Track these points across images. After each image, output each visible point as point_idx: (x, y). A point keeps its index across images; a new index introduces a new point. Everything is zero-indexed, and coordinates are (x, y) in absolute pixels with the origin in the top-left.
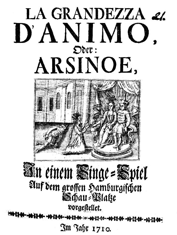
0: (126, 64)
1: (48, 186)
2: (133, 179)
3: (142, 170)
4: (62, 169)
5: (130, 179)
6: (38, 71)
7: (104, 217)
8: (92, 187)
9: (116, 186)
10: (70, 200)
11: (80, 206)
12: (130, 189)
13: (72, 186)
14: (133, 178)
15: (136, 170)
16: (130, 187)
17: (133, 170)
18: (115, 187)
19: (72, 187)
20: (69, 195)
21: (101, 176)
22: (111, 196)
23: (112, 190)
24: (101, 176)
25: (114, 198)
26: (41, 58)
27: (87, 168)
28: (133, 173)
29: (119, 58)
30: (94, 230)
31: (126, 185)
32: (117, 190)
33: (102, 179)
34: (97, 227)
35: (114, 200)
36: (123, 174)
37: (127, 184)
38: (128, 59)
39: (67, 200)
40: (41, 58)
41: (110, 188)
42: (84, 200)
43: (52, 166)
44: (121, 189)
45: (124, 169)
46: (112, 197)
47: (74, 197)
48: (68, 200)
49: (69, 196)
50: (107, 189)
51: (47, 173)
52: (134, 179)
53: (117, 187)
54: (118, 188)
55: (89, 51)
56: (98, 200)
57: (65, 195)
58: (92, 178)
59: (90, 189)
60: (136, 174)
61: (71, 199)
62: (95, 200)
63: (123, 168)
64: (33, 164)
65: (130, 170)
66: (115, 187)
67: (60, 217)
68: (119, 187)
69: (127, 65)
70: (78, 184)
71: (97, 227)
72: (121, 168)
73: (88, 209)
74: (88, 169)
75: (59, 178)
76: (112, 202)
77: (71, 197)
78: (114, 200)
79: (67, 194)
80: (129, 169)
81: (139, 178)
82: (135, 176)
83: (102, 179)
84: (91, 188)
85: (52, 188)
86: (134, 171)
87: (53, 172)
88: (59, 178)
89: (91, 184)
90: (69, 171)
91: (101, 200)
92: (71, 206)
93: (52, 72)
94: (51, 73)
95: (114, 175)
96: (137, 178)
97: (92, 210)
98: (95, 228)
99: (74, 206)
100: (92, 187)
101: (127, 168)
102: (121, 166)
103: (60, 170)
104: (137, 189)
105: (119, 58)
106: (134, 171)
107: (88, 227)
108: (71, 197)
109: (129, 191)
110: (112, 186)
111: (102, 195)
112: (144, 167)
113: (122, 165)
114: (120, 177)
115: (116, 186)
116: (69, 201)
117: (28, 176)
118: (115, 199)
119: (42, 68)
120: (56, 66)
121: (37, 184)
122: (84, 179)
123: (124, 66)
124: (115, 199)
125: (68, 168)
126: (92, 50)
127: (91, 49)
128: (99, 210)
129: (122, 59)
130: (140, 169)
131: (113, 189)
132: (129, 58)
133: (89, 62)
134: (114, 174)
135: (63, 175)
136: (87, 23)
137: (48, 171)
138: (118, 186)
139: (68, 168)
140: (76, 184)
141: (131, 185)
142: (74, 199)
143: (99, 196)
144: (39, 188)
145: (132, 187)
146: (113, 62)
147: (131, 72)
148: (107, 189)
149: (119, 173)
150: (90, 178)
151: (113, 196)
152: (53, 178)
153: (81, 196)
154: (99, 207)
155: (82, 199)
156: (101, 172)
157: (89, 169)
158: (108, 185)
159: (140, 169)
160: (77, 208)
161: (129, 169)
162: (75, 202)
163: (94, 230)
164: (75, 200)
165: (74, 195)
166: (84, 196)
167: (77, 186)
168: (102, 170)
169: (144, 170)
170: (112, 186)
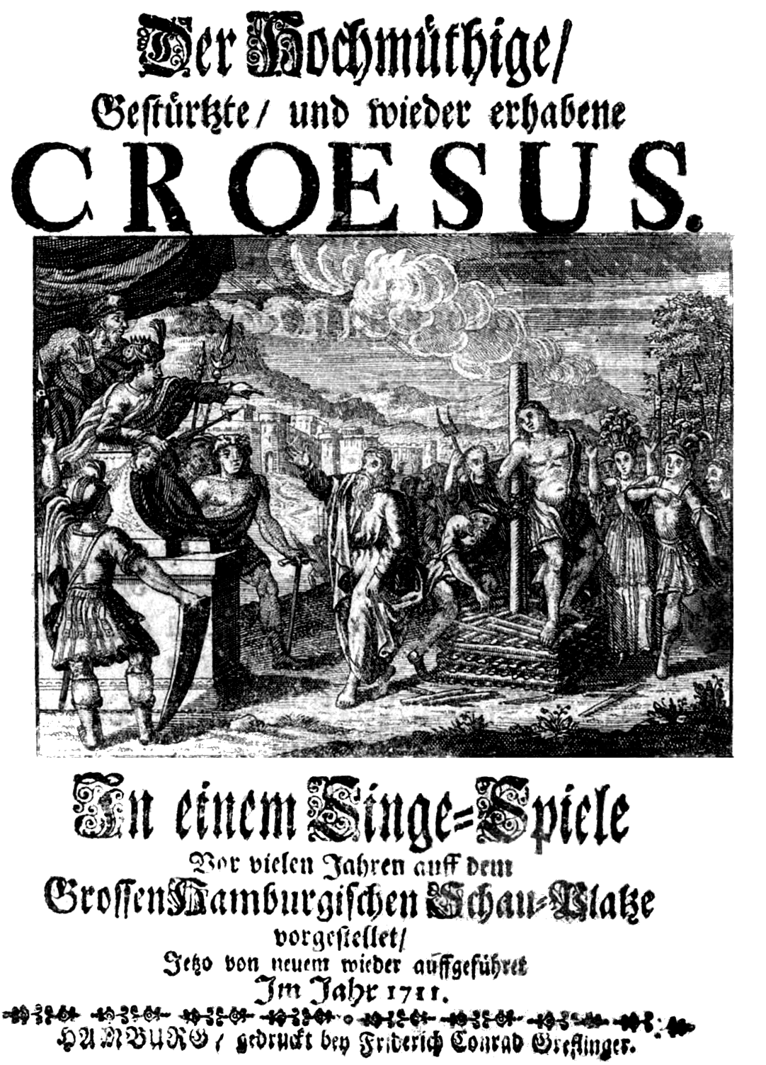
3: (586, 803)
4: (250, 798)
7: (425, 1013)
10: (458, 913)
13: (105, 890)
14: (548, 837)
19: (104, 894)
20: (453, 891)
21: (516, 63)
22: (635, 894)
24: (516, 63)
25: (644, 904)
27: (354, 793)
28: (547, 811)
30: (391, 997)
31: (349, 888)
32: (307, 912)
33: (519, 77)
34: (403, 988)
35: (647, 913)
39: (447, 917)
41: (276, 901)
43: (206, 784)
46: (639, 901)
47: (476, 901)
48: (449, 914)
50: (261, 906)
51: (180, 817)
54: (313, 904)
55: (218, 59)
56: (574, 915)
57: (437, 893)
58: (377, 836)
61: (465, 911)
62: (560, 911)
63: (501, 794)
64: (114, 780)
65: (532, 799)
70: (133, 882)
71: (403, 988)
74: (357, 798)
76: (636, 921)
77: (465, 900)
78: (647, 913)
80: (527, 794)
82: (552, 826)
83: (421, 842)
85: (589, 116)
86: (551, 803)
87: (210, 807)
88: (238, 835)
91: (588, 913)
96: (566, 835)
98: (397, 992)
102: (492, 784)
103: (239, 800)
106: (551, 803)
107: (468, 106)
108: (465, 900)
111: (594, 891)
113: (326, 779)
115: (304, 893)
116: (455, 916)
117: (93, 835)
118: (626, 830)
124: (626, 830)
126: (466, 115)
127: (227, 42)
131: (289, 907)
134: (461, 820)
135: (254, 819)
138: (313, 894)
140: (122, 882)
141: (371, 888)
143: (578, 896)
148: (261, 906)
150: (369, 834)
151: (641, 894)
155: (515, 907)
156: (517, 42)
157: (364, 796)
159: (409, 104)
160: (309, 939)
161: (527, 794)
162: (483, 922)
163: (391, 997)
164: (481, 912)
167: (128, 891)
168: (422, 801)
169: (593, 801)
170: (285, 894)
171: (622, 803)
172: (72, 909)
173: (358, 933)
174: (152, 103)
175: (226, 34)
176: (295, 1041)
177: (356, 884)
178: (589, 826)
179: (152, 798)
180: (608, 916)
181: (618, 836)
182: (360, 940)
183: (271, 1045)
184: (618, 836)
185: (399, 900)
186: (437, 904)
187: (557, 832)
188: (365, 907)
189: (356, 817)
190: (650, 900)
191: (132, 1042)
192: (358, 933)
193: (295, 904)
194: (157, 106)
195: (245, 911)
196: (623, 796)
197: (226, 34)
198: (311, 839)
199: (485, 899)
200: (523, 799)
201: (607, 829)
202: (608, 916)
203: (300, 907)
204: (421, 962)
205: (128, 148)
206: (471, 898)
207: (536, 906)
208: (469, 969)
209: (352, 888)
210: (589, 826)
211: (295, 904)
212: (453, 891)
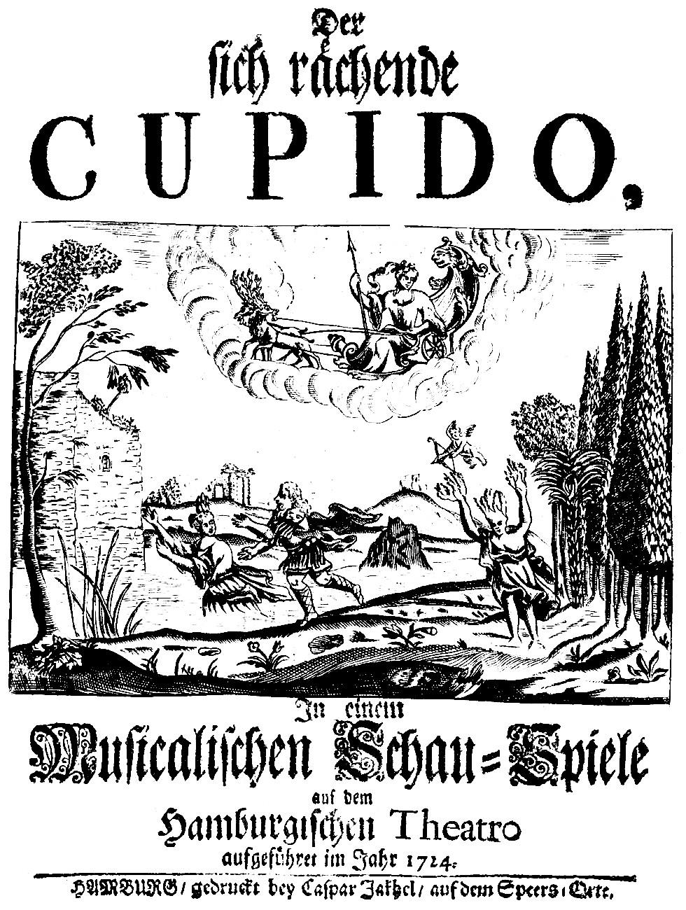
2: (572, 782)
3: (610, 746)
5: (562, 783)
8: (176, 824)
9: (272, 818)
15: (585, 745)
16: (327, 825)
17: (572, 745)
18: (268, 823)
23: (254, 836)
28: (575, 754)
30: (410, 865)
34: (419, 858)
36: (532, 762)
44: (290, 831)
45: (361, 739)
50: (233, 831)
52: (577, 781)
53: (276, 823)
59: (165, 831)
60: (424, 762)
65: (562, 744)
66: (268, 823)
67: (411, 876)
71: (419, 858)
73: (627, 778)
75: (149, 775)
81: (599, 778)
84: (170, 829)
89: (171, 810)
90: (295, 746)
95: (498, 765)
96: (592, 780)
97: (230, 892)
100: (176, 824)
101: (373, 733)
102: (525, 731)
110: (253, 819)
112: (619, 735)
114: (519, 775)
115: (272, 818)
122: (539, 782)
124: (646, 771)
125: (568, 742)
127: (300, 63)
128: (285, 739)
130: (601, 742)
131: (258, 831)
134: (494, 761)
136: (419, 115)
137: (608, 754)
139: (568, 742)
144: (241, 863)
149: (517, 757)
152: (450, 779)
158: (238, 814)
159: (601, 742)
161: (557, 740)
163: (410, 865)
169: (617, 744)
170: (253, 819)
171: (643, 749)
175: (299, 57)
177: (318, 811)
178: (613, 765)
179: (310, 742)
181: (638, 778)
185: (311, 859)
187: (584, 776)
189: (555, 761)
191: (123, 891)
193: (304, 829)
195: (219, 836)
196: (160, 737)
197: (299, 57)
198: (514, 783)
201: (628, 771)
203: (268, 831)
204: (228, 854)
205: (252, 117)
207: (477, 764)
208: (267, 861)
210: (613, 765)
211: (304, 829)
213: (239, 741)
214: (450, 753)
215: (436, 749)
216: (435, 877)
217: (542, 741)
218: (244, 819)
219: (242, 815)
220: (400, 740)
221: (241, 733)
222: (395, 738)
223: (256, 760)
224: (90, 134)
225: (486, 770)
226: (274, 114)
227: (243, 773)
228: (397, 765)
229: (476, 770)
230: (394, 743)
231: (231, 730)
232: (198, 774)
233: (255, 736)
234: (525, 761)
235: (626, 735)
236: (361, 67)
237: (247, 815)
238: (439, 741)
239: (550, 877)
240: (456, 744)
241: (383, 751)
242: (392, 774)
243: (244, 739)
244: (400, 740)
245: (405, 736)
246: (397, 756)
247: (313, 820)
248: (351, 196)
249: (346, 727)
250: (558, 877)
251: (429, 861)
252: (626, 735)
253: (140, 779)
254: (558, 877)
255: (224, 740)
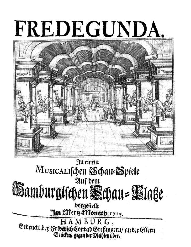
0: (48, 28)
1: (91, 180)
6: (151, 36)
11: (59, 189)
12: (71, 195)
18: (51, 191)
20: (122, 169)
24: (58, 195)
26: (153, 22)
29: (41, 22)
33: (59, 198)
34: (113, 213)
37: (73, 167)
38: (50, 23)
40: (153, 22)
42: (110, 174)
47: (100, 171)
48: (121, 174)
49: (95, 170)
63: (96, 188)
66: (51, 191)
68: (83, 205)
69: (49, 29)
72: (94, 188)
79: (94, 168)
83: (59, 198)
90: (35, 190)
92: (77, 204)
93: (73, 35)
94: (42, 36)
99: (79, 204)
104: (82, 172)
105: (41, 22)
109: (74, 174)
111: (145, 189)
118: (139, 173)
119: (155, 32)
120: (32, 29)
121: (82, 180)
123: (77, 30)
124: (139, 173)
129: (75, 23)
132: (82, 22)
133: (121, 26)
138: (82, 205)
142: (100, 173)
144: (83, 183)
145: (77, 170)
146: (66, 26)
147: (84, 36)
153: (107, 170)
154: (99, 205)
155: (108, 172)
160: (82, 206)
162: (101, 176)
163: (111, 215)
165: (100, 169)
166: (110, 170)
172: (58, 236)
173: (93, 205)
174: (90, 205)
176: (64, 235)
180: (127, 169)
181: (138, 174)
182: (93, 207)
183: (59, 236)
184: (138, 174)
186: (92, 172)
188: (75, 173)
190: (138, 171)
192: (93, 205)
194: (91, 205)
199: (102, 170)
200: (101, 190)
202: (127, 169)
206: (99, 171)
207: (113, 172)
209: (67, 188)
210: (133, 172)
212: (95, 169)
213: (70, 190)
214: (118, 193)
215: (114, 192)
216: (128, 218)
217: (98, 189)
218: (43, 189)
219: (42, 187)
220: (106, 190)
221: (71, 188)
222: (105, 190)
223: (75, 195)
224: (52, 24)
225: (126, 196)
226: (138, 22)
227: (71, 197)
228: (105, 196)
229: (124, 196)
230: (105, 191)
231: (68, 187)
232: (31, 196)
233: (74, 189)
234: (94, 194)
235: (146, 188)
236: (109, 192)
237: (44, 187)
238: (115, 190)
239: (121, 218)
240: (119, 191)
241: (102, 192)
242: (104, 198)
243: (72, 190)
244: (106, 190)
245: (107, 189)
246: (105, 194)
247: (72, 169)
248: (107, 21)
249: (93, 186)
250: (119, 218)
251: (116, 214)
252: (146, 188)
253: (26, 197)
254: (119, 218)
255: (66, 190)
